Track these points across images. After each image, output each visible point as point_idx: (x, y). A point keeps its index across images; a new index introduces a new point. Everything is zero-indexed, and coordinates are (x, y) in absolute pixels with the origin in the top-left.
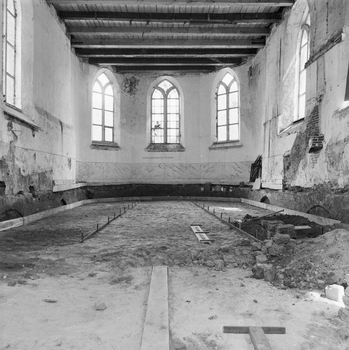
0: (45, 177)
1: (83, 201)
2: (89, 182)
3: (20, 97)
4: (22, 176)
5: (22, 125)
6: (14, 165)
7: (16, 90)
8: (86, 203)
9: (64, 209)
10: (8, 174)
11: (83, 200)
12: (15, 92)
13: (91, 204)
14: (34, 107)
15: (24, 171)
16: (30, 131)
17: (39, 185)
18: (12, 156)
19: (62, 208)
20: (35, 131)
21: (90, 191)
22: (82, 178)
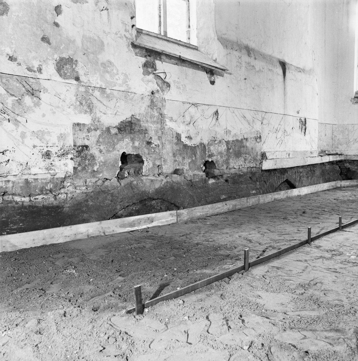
0: (244, 147)
1: (334, 182)
2: (349, 154)
3: (195, 27)
4: (185, 146)
5: (184, 66)
6: (162, 128)
7: (190, 19)
8: (339, 186)
9: (286, 195)
10: (149, 143)
11: (334, 180)
12: (189, 21)
13: (347, 187)
14: (216, 38)
15: (190, 138)
16: (203, 76)
17: (228, 160)
18: (156, 114)
19: (282, 195)
20: (215, 76)
21: (349, 168)
22: (338, 148)
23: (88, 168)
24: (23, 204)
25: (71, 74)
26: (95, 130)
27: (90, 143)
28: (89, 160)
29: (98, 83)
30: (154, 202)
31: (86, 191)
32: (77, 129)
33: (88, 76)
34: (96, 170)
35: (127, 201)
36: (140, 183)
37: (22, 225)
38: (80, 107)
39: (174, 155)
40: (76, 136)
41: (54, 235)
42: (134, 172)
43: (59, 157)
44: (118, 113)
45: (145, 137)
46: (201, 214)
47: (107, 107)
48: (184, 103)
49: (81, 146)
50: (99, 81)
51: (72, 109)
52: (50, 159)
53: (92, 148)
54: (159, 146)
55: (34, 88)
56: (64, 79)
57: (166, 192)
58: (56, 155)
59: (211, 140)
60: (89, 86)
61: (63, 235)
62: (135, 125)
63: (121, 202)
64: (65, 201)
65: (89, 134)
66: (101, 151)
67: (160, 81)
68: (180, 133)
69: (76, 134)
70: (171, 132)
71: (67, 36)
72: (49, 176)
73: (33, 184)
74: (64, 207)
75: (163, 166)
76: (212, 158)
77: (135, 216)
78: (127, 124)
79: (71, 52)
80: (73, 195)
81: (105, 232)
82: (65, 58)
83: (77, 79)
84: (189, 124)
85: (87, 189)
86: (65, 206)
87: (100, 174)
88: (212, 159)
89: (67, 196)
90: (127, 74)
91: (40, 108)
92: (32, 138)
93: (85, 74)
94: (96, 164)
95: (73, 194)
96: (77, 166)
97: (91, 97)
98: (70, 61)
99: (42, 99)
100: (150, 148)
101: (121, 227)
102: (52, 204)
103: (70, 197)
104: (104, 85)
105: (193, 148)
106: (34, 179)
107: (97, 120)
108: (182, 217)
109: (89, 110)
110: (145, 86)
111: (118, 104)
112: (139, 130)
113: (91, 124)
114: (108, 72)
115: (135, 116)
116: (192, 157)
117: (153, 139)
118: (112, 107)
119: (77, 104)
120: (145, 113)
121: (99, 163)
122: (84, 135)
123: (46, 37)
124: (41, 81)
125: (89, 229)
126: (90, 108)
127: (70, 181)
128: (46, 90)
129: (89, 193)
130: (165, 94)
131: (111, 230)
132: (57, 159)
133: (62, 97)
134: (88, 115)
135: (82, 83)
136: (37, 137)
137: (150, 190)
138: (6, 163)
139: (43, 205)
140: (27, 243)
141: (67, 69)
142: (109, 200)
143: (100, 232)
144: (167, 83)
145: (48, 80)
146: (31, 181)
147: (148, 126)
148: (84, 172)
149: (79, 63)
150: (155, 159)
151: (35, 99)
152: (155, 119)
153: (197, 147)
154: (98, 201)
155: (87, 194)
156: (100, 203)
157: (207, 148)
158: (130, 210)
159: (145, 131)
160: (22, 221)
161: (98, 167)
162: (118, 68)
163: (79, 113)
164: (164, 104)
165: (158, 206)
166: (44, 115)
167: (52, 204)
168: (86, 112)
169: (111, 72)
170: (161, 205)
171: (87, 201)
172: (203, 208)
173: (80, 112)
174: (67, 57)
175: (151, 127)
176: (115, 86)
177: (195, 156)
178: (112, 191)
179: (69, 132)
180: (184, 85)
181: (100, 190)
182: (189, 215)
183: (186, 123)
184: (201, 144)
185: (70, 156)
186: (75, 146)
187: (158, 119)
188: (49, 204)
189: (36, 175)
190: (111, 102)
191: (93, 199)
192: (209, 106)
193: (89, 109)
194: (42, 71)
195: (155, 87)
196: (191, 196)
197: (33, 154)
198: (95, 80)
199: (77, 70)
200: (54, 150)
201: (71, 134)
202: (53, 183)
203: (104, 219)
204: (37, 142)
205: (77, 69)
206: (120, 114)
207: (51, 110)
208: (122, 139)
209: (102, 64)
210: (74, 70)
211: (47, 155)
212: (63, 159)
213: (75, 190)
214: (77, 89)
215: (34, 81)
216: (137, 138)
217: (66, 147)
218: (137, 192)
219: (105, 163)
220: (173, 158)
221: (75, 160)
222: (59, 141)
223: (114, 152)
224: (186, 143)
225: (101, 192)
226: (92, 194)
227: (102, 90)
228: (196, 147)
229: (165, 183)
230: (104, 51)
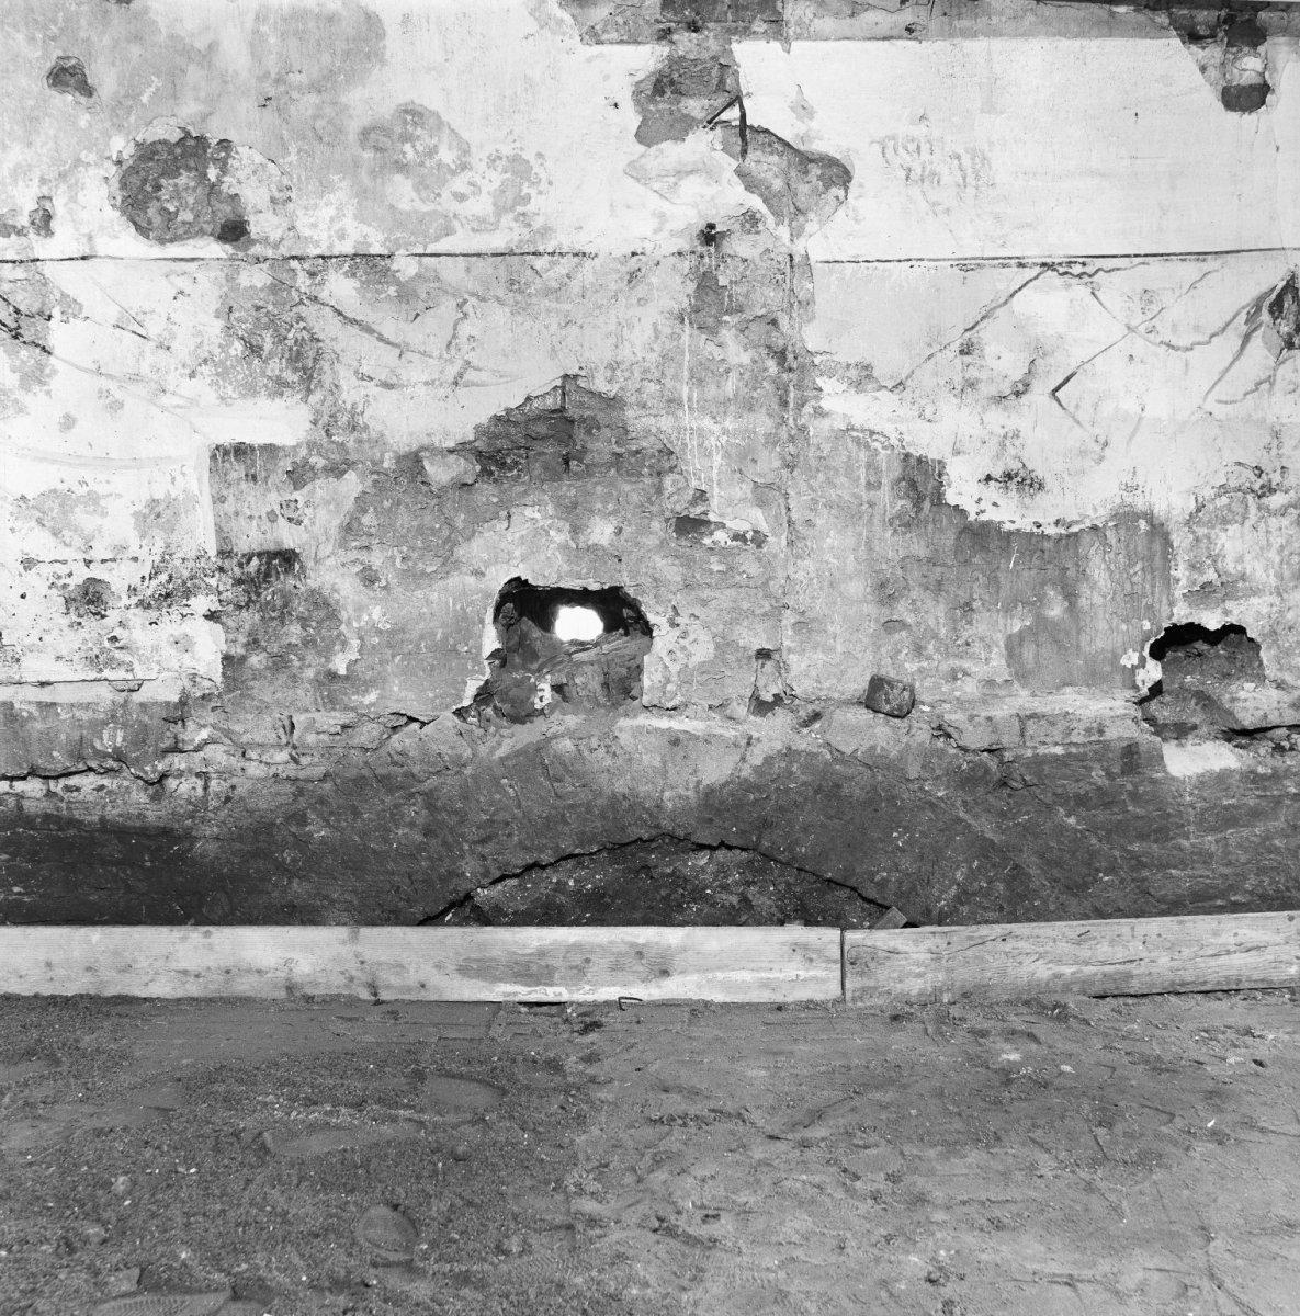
4: (981, 537)
10: (690, 526)
15: (1020, 480)
23: (302, 659)
24: (20, 808)
25: (197, 216)
26: (336, 471)
27: (305, 537)
28: (304, 622)
29: (342, 236)
30: (702, 859)
31: (291, 770)
32: (233, 476)
33: (290, 206)
34: (342, 672)
35: (520, 842)
36: (592, 750)
37: (19, 894)
38: (249, 364)
39: (885, 592)
40: (229, 507)
41: (135, 961)
42: (606, 685)
43: (149, 606)
44: (470, 375)
45: (659, 490)
46: (1067, 970)
47: (402, 349)
48: (965, 266)
49: (259, 555)
50: (348, 223)
51: (208, 380)
52: (103, 617)
53: (317, 561)
54: (759, 539)
55: (22, 308)
56: (162, 241)
57: (781, 809)
58: (134, 600)
59: (1223, 489)
60: (293, 257)
61: (174, 965)
62: (589, 432)
63: (483, 841)
64: (198, 807)
65: (297, 495)
66: (369, 578)
67: (775, 158)
68: (932, 455)
69: (231, 499)
70: (863, 455)
71: (172, 37)
72: (104, 695)
73: (39, 726)
74: (197, 839)
75: (792, 659)
76: (1229, 605)
77: (577, 923)
78: (542, 429)
79: (189, 110)
80: (233, 787)
81: (380, 983)
82: (165, 142)
83: (234, 232)
84: (1018, 394)
85: (295, 761)
86: (200, 833)
87: (366, 691)
88: (1226, 612)
89: (206, 788)
90: (529, 155)
91: (48, 393)
92: (18, 525)
93: (273, 200)
94: (344, 644)
95: (234, 780)
96: (240, 651)
97: (308, 311)
98: (192, 151)
99: (56, 351)
100: (698, 554)
101: (464, 970)
102: (141, 816)
103: (217, 795)
104: (381, 237)
105: (1047, 545)
106: (39, 704)
107: (343, 420)
108: (883, 976)
109: (296, 378)
110: (654, 202)
111: (466, 329)
112: (619, 455)
113: (312, 445)
114: (401, 167)
115: (582, 383)
116: (1037, 603)
117: (715, 503)
118: (436, 346)
119: (233, 352)
120: (653, 357)
121: (361, 638)
122: (274, 499)
123: (73, 62)
124: (48, 269)
125: (295, 956)
126: (304, 366)
127: (211, 718)
128: (72, 308)
129: (309, 780)
130: (809, 228)
131: (412, 978)
132: (138, 618)
133: (154, 328)
134: (292, 399)
135: (257, 250)
136: (40, 522)
137: (667, 794)
138: (224, 619)
139: (103, 820)
140: (23, 973)
141: (177, 194)
142: (412, 825)
143: (352, 979)
144: (829, 162)
145: (83, 258)
146: (25, 714)
147: (680, 430)
148: (282, 678)
149: (240, 149)
150: (736, 615)
151: (24, 353)
152: (731, 385)
153: (1086, 539)
154: (359, 824)
155: (301, 784)
156: (363, 834)
157: (1181, 539)
158: (544, 890)
159: (665, 459)
160: (22, 878)
161: (355, 656)
162: (465, 135)
163: (243, 396)
164: (803, 288)
165: (725, 888)
166: (68, 422)
167: (141, 816)
168: (280, 386)
169: (422, 164)
170: (748, 884)
171: (301, 820)
172: (1083, 938)
173: (250, 390)
174: (175, 136)
175: (701, 433)
176: (448, 231)
177: (1071, 596)
178: (433, 782)
179: (194, 488)
180: (973, 153)
181: (365, 772)
182: (949, 970)
183: (987, 390)
184: (1125, 518)
185: (202, 603)
186: (224, 553)
187: (755, 383)
188: (129, 816)
189: (47, 688)
190: (429, 319)
191: (331, 813)
192: (1212, 264)
193: (295, 370)
194: (53, 223)
195: (727, 197)
196: (985, 848)
197: (23, 597)
198: (329, 220)
199: (232, 191)
200: (119, 578)
201: (206, 500)
202: (125, 726)
203: (395, 917)
204: (39, 543)
205: (229, 185)
206: (483, 376)
207: (103, 393)
208: (504, 510)
209: (365, 133)
210: (213, 189)
211: (91, 598)
212: (166, 618)
213: (239, 763)
214: (229, 278)
215: (19, 273)
216: (605, 503)
217: (178, 563)
218: (584, 796)
219: (393, 639)
220: (870, 609)
221: (230, 623)
222: (143, 537)
223: (454, 581)
224: (983, 517)
225: (364, 785)
226: (328, 786)
227: (370, 265)
228: (1076, 535)
229: (768, 760)
230: (383, 62)
